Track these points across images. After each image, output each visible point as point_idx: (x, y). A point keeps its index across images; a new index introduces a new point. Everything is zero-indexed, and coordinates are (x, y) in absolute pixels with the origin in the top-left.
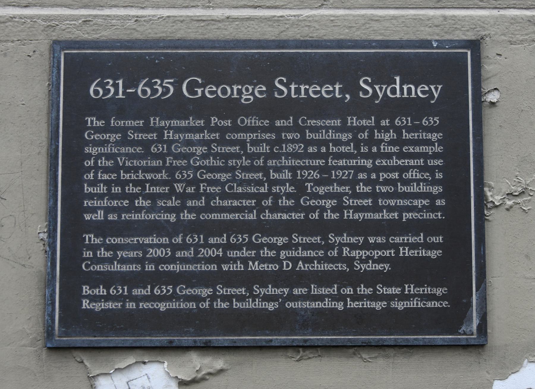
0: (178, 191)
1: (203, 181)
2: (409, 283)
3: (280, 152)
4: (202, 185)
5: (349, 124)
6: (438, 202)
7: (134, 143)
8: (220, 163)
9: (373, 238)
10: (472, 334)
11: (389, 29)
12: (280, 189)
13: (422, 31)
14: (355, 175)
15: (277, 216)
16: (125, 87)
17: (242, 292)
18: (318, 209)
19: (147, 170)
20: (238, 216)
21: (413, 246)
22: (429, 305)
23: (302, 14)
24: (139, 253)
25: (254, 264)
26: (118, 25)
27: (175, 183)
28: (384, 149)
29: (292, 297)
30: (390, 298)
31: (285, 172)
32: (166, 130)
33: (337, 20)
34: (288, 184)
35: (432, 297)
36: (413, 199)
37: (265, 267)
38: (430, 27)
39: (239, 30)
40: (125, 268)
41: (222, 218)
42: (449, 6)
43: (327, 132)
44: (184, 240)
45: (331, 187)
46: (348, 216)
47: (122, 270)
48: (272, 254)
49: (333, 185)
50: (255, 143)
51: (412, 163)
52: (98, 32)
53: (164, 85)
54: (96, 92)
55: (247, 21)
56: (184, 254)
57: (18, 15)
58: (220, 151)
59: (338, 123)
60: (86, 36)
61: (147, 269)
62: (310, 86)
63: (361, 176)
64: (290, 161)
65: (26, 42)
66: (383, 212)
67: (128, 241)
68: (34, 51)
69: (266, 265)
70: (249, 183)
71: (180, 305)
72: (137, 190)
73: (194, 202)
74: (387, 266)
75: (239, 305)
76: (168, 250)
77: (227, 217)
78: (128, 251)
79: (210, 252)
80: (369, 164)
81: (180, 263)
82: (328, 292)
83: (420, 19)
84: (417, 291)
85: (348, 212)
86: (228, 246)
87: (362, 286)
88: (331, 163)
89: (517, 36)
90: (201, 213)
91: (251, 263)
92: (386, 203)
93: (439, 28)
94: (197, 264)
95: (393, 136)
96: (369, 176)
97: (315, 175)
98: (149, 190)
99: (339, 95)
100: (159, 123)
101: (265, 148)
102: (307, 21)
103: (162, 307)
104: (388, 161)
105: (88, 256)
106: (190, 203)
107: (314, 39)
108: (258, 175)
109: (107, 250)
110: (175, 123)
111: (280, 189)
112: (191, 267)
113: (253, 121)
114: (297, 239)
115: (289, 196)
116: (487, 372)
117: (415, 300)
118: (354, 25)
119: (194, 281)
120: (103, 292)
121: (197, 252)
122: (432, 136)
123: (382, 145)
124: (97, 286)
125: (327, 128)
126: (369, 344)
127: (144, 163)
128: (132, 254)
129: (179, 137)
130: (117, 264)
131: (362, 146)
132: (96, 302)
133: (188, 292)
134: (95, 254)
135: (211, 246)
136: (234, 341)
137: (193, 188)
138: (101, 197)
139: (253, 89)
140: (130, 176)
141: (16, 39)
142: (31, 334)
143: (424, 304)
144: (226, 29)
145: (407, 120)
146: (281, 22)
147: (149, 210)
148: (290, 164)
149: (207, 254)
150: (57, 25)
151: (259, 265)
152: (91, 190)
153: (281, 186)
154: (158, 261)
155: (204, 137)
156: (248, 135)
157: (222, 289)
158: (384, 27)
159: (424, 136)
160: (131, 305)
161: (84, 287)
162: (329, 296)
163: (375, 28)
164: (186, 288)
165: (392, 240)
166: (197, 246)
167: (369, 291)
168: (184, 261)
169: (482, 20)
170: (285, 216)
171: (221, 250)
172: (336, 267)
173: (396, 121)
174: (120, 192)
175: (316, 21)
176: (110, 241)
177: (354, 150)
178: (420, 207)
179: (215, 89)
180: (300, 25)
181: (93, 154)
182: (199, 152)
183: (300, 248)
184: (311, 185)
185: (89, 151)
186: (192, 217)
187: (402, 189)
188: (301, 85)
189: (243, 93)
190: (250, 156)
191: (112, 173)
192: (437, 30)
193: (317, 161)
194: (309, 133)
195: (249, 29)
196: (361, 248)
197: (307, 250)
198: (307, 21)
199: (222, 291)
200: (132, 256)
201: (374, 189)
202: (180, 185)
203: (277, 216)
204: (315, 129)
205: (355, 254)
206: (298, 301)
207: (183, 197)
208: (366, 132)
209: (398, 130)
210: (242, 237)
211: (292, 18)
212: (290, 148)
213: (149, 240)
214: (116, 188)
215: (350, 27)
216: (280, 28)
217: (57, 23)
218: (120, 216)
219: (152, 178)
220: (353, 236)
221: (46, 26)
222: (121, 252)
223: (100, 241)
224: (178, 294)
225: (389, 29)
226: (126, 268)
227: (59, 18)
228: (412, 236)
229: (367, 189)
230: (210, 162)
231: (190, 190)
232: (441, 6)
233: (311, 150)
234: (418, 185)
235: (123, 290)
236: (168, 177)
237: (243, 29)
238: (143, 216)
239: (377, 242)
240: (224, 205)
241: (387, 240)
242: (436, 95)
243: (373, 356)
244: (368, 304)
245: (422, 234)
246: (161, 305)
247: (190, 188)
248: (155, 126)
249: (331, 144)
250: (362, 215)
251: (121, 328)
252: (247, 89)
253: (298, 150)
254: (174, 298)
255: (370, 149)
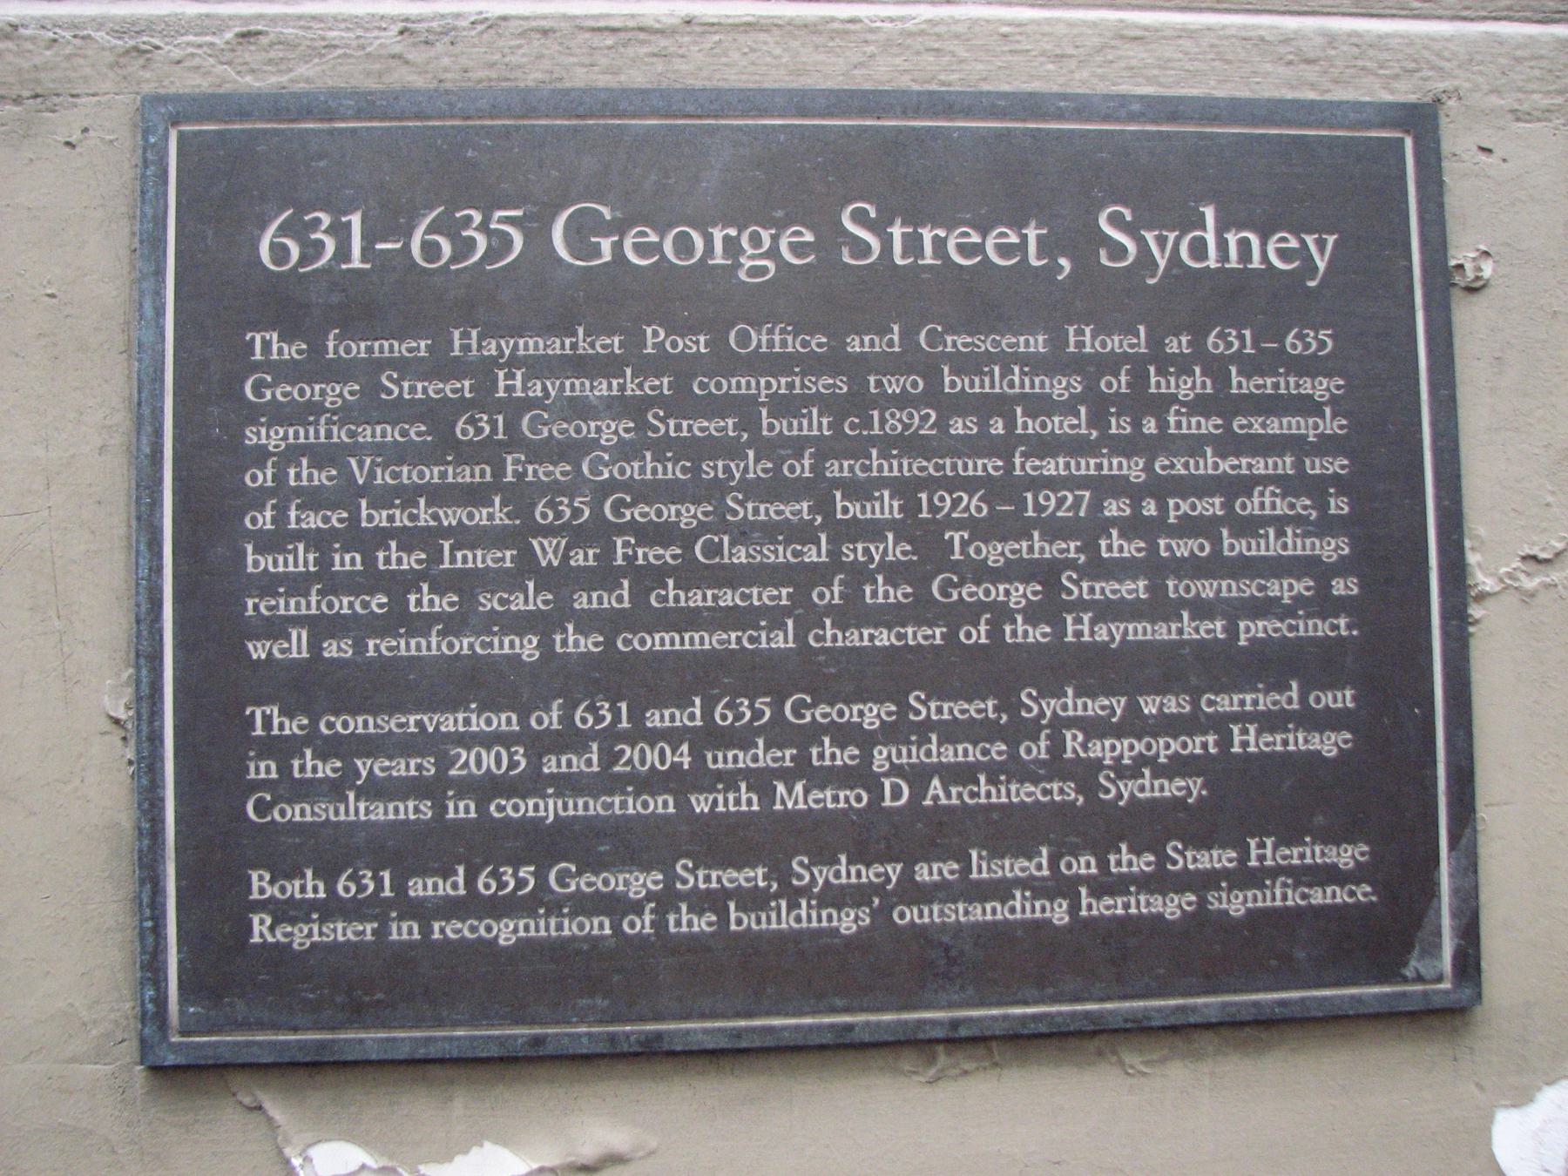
0: (544, 564)
1: (621, 530)
2: (1262, 833)
3: (865, 433)
4: (619, 543)
5: (1072, 349)
6: (1339, 587)
7: (399, 412)
8: (674, 471)
9: (1154, 701)
10: (1440, 979)
11: (1170, 65)
12: (867, 551)
13: (1268, 73)
14: (1097, 506)
15: (858, 638)
16: (369, 238)
17: (755, 878)
18: (985, 612)
19: (439, 495)
20: (739, 639)
21: (1271, 721)
22: (1318, 897)
23: (914, 15)
24: (426, 764)
25: (790, 792)
26: (347, 46)
27: (534, 537)
28: (1179, 425)
29: (915, 893)
30: (1205, 882)
31: (881, 498)
32: (501, 367)
33: (1020, 34)
34: (890, 536)
35: (1329, 875)
36: (1267, 578)
37: (828, 798)
38: (1290, 63)
39: (724, 60)
40: (381, 812)
41: (687, 647)
42: (1329, 10)
43: (1007, 371)
44: (567, 719)
45: (1025, 544)
46: (1078, 634)
47: (372, 817)
48: (847, 756)
49: (1031, 538)
50: (785, 406)
51: (1260, 466)
52: (283, 67)
53: (492, 226)
54: (280, 253)
55: (746, 32)
56: (569, 764)
57: (32, 18)
58: (676, 431)
59: (1038, 343)
60: (248, 79)
61: (451, 815)
62: (950, 229)
63: (1112, 508)
64: (895, 463)
65: (56, 100)
66: (1180, 619)
67: (391, 724)
68: (85, 130)
69: (829, 793)
70: (770, 532)
71: (560, 927)
72: (411, 561)
73: (595, 595)
74: (1195, 783)
75: (749, 921)
76: (516, 752)
77: (702, 643)
78: (391, 758)
79: (652, 757)
80: (1134, 470)
81: (557, 795)
82: (1023, 870)
83: (1262, 39)
84: (1285, 858)
85: (1078, 621)
86: (710, 737)
87: (1124, 847)
88: (1023, 467)
89: (1535, 96)
90: (618, 633)
91: (781, 788)
92: (1187, 589)
93: (1317, 68)
94: (611, 793)
95: (1204, 385)
96: (1136, 505)
97: (974, 505)
98: (453, 560)
99: (1039, 258)
100: (480, 348)
101: (816, 424)
102: (929, 34)
103: (506, 932)
104: (1192, 462)
105: (263, 776)
106: (585, 599)
107: (952, 89)
108: (798, 507)
109: (321, 755)
110: (530, 345)
111: (867, 551)
112: (591, 803)
113: (777, 338)
114: (923, 708)
115: (894, 573)
116: (1477, 1085)
117: (1278, 884)
118: (1070, 51)
119: (602, 849)
120: (315, 890)
121: (610, 758)
122: (1314, 387)
123: (1172, 410)
124: (296, 873)
125: (1006, 361)
126: (1145, 1024)
127: (432, 474)
128: (403, 766)
129: (544, 389)
130: (357, 799)
131: (1112, 415)
132: (293, 921)
133: (585, 883)
134: (285, 769)
135: (653, 737)
136: (738, 1034)
137: (591, 552)
138: (297, 585)
139: (775, 239)
140: (391, 518)
141: (26, 93)
142: (95, 1022)
143: (1304, 896)
144: (683, 56)
145: (1241, 338)
146: (853, 38)
147: (453, 625)
148: (896, 473)
149: (643, 762)
150: (157, 48)
151: (807, 791)
152: (266, 562)
153: (872, 541)
154: (488, 788)
155: (622, 388)
156: (763, 381)
157: (693, 871)
158: (1159, 59)
159: (1290, 385)
160: (404, 931)
161: (255, 876)
162: (1023, 883)
163: (1134, 63)
164: (579, 873)
165: (1211, 703)
166: (610, 737)
167: (1144, 863)
168: (568, 785)
169: (1436, 46)
170: (885, 636)
171: (685, 748)
172: (1046, 792)
173: (1211, 339)
174: (359, 567)
175: (957, 36)
176: (330, 725)
177: (1089, 426)
178: (1286, 601)
179: (653, 238)
180: (908, 47)
181: (271, 449)
182: (609, 438)
183: (934, 738)
184: (962, 537)
185: (259, 439)
186: (589, 644)
187: (1232, 546)
188: (924, 226)
189: (742, 251)
190: (768, 448)
191: (334, 507)
192: (1310, 73)
193: (980, 462)
194: (950, 375)
195: (752, 57)
196: (1119, 732)
197: (954, 742)
198: (929, 34)
199: (691, 877)
200: (403, 773)
201: (1153, 548)
202: (550, 543)
203: (861, 635)
204: (968, 364)
205: (1099, 749)
206: (930, 902)
207: (560, 580)
208: (1123, 372)
209: (1216, 368)
210: (751, 706)
211: (885, 25)
212: (895, 422)
213: (456, 721)
214: (347, 557)
215: (1057, 56)
216: (848, 54)
217: (156, 41)
218: (360, 647)
219: (460, 521)
220: (1094, 696)
221: (122, 50)
222: (369, 763)
223: (301, 727)
224: (552, 892)
225: (1170, 65)
226: (386, 813)
227: (163, 26)
228: (1266, 692)
229: (1132, 549)
230: (642, 470)
231: (583, 558)
232: (1306, 9)
233: (958, 427)
234: (1281, 534)
235: (379, 881)
236: (510, 519)
237: (735, 56)
238: (433, 645)
239: (1166, 710)
240: (691, 604)
241: (1195, 703)
242: (1321, 265)
243: (1155, 1057)
244: (1145, 904)
245: (1294, 685)
246: (502, 926)
247: (581, 552)
248: (510, 395)
249: (1019, 411)
250: (1118, 628)
251: (379, 1001)
252: (756, 240)
253: (920, 427)
254: (541, 904)
255: (1137, 424)
